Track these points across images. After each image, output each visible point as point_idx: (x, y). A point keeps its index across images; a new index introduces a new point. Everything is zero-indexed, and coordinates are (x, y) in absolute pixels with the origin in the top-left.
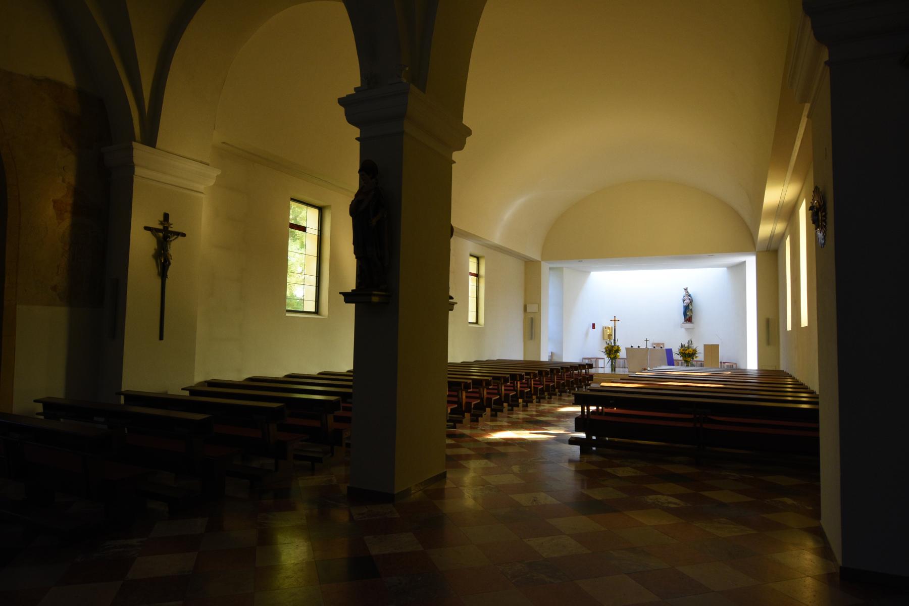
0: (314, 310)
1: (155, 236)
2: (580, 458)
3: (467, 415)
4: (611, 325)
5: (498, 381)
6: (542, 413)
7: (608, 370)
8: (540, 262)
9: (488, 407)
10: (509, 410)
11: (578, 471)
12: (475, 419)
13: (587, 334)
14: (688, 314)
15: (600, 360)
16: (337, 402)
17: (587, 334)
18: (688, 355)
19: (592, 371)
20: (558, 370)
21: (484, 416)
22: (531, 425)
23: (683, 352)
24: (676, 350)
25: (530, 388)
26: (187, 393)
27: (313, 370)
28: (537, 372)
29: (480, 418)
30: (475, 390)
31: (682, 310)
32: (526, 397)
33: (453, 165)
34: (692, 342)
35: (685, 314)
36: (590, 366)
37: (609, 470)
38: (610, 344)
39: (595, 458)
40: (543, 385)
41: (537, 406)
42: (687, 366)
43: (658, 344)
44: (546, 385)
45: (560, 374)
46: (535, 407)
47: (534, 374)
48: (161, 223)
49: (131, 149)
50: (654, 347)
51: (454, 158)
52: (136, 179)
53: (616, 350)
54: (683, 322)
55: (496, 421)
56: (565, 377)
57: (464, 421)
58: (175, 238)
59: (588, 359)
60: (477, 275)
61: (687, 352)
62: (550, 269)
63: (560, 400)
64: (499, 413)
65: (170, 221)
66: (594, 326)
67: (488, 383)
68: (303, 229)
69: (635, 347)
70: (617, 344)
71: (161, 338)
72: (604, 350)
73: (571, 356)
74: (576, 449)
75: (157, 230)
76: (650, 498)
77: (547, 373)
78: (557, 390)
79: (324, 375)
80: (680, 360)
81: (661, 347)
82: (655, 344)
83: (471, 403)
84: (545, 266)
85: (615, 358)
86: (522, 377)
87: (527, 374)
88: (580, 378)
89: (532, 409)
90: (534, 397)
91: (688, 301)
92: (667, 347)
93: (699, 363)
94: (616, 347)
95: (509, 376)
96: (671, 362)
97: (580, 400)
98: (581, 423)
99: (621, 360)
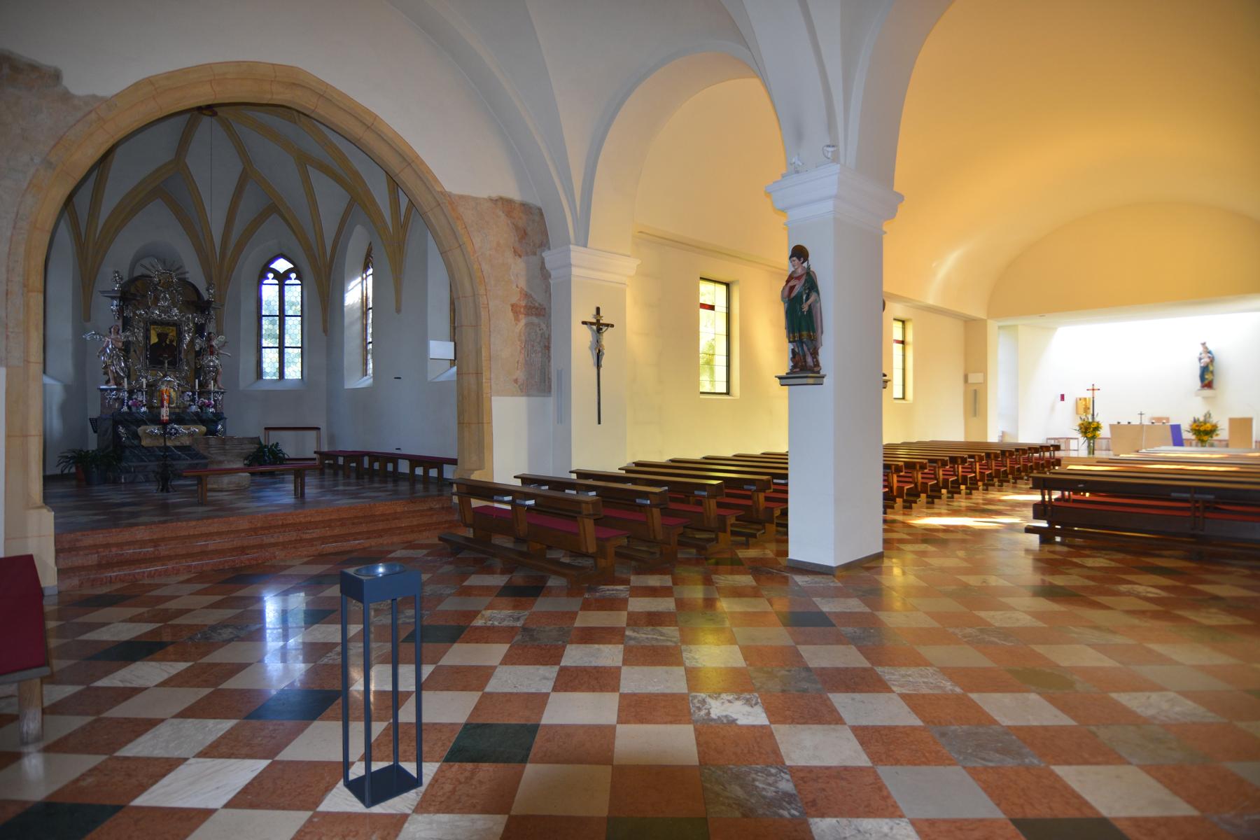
0: (725, 391)
1: (591, 329)
2: (1040, 547)
3: (899, 500)
4: (1089, 395)
5: (935, 465)
6: (991, 502)
7: (1083, 453)
8: (985, 321)
9: (923, 493)
10: (948, 498)
11: (1037, 560)
12: (908, 506)
13: (1053, 408)
14: (1207, 377)
15: (1071, 441)
16: (768, 481)
17: (1053, 408)
18: (1204, 432)
19: (1058, 454)
20: (1011, 453)
21: (918, 502)
22: (977, 513)
23: (1197, 428)
24: (1185, 425)
25: (975, 472)
26: (574, 476)
27: (728, 453)
28: (983, 454)
29: (913, 505)
30: (907, 475)
31: (1197, 372)
32: (971, 484)
33: (884, 236)
34: (1210, 415)
35: (1202, 378)
36: (1057, 448)
37: (1075, 560)
38: (1086, 420)
39: (1058, 548)
40: (991, 469)
41: (984, 493)
42: (1202, 446)
43: (1159, 419)
44: (996, 470)
45: (1014, 457)
46: (981, 495)
47: (980, 456)
48: (595, 317)
49: (569, 251)
50: (1153, 423)
51: (885, 229)
52: (573, 279)
53: (1096, 428)
55: (933, 508)
56: (1022, 460)
57: (896, 506)
59: (1054, 439)
60: (903, 342)
61: (1202, 429)
62: (1000, 327)
63: (1015, 488)
64: (936, 500)
65: (601, 314)
66: (1062, 397)
67: (923, 467)
68: (712, 308)
69: (1124, 422)
70: (1097, 419)
71: (599, 423)
72: (1078, 428)
73: (1030, 434)
74: (1035, 538)
75: (592, 324)
76: (1123, 588)
77: (996, 456)
78: (1010, 476)
79: (738, 457)
80: (1193, 440)
81: (1164, 423)
82: (1154, 418)
83: (903, 487)
84: (992, 326)
85: (1094, 437)
86: (964, 460)
87: (971, 457)
88: (1041, 462)
89: (978, 497)
90: (980, 483)
91: (1206, 360)
92: (1173, 422)
93: (1224, 443)
94: (1095, 424)
95: (948, 458)
96: (1178, 440)
97: (1042, 485)
98: (1040, 510)
99: (1104, 441)
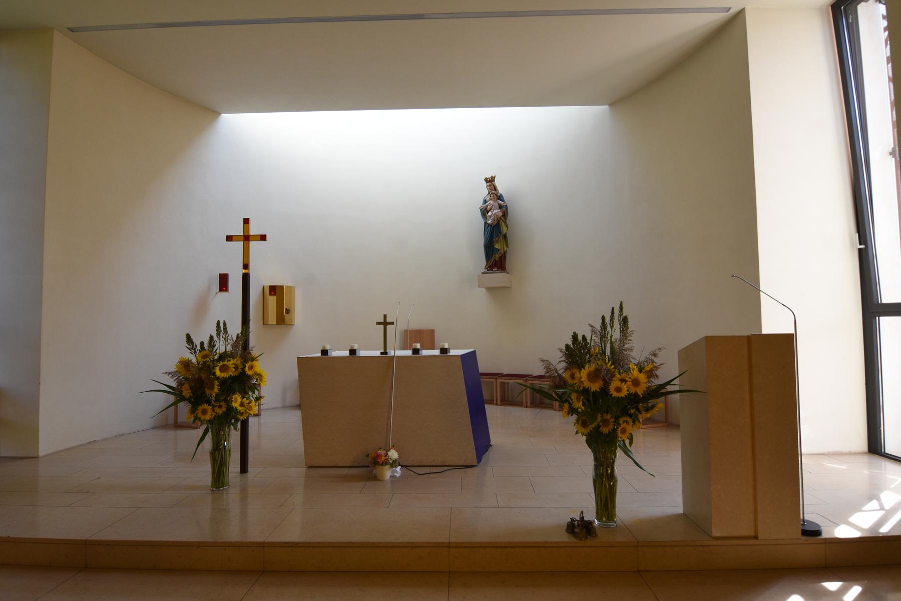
23: (595, 387)
35: (489, 249)
54: (484, 270)
58: (890, 99)
91: (496, 212)
